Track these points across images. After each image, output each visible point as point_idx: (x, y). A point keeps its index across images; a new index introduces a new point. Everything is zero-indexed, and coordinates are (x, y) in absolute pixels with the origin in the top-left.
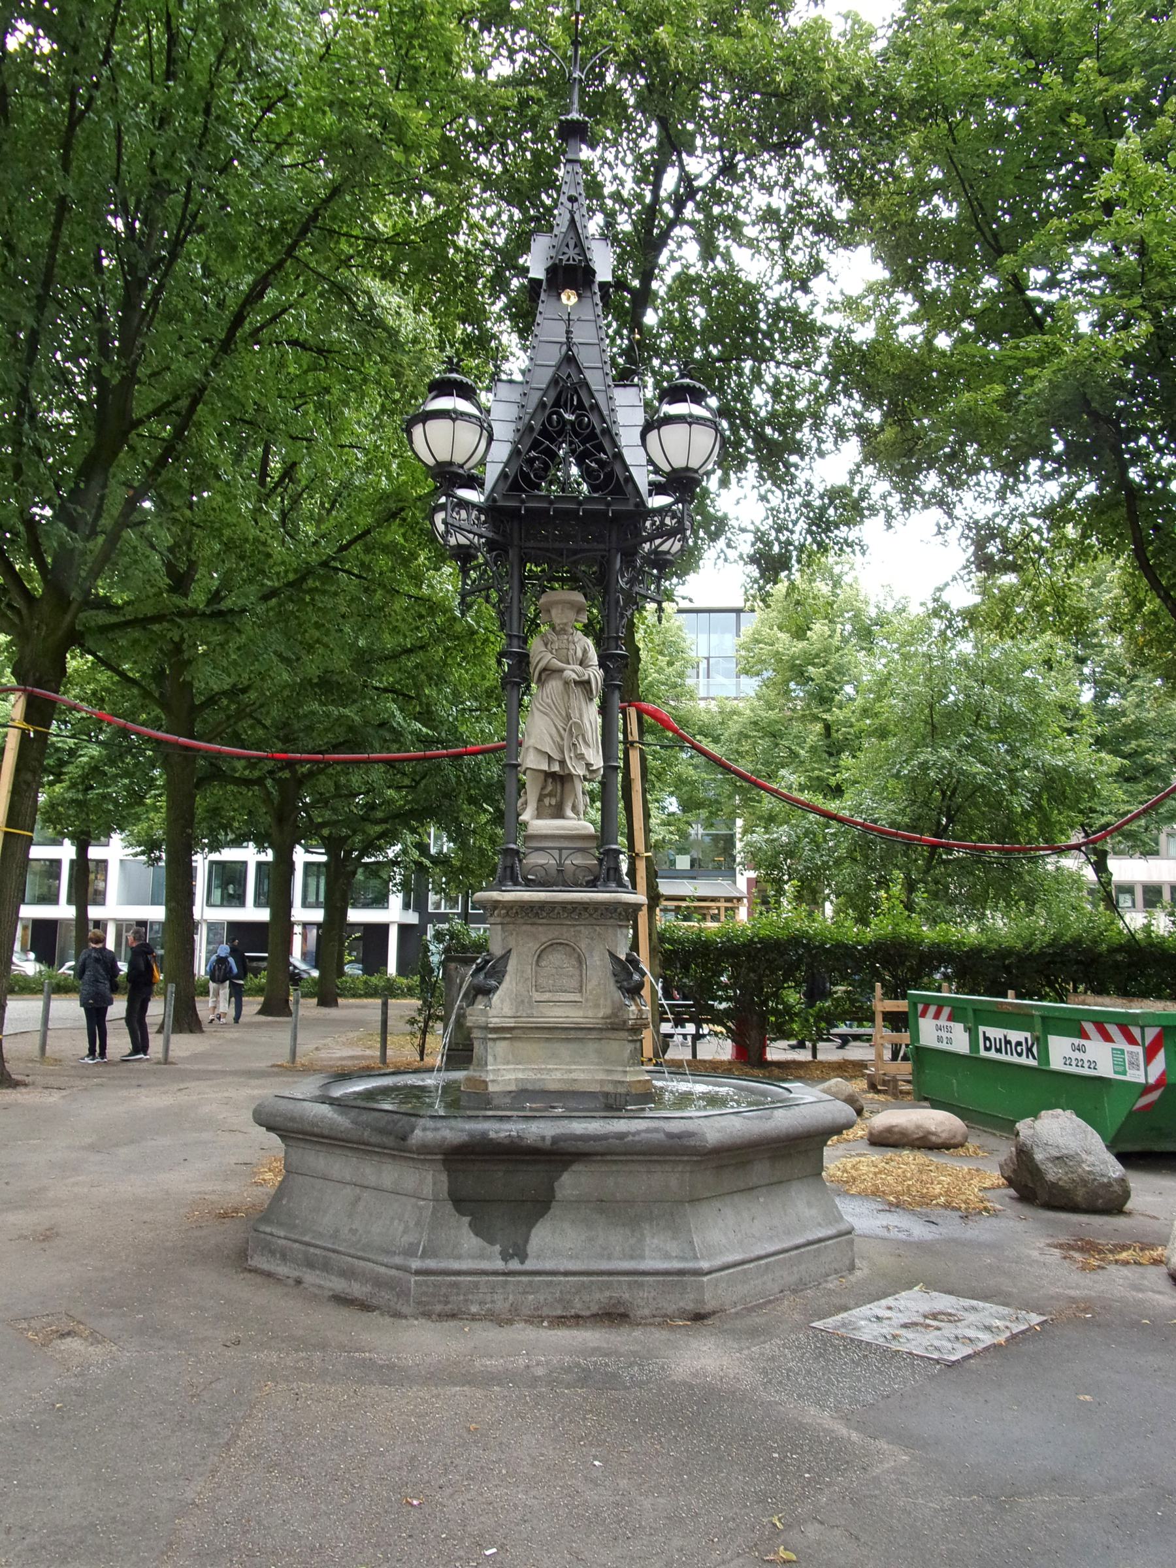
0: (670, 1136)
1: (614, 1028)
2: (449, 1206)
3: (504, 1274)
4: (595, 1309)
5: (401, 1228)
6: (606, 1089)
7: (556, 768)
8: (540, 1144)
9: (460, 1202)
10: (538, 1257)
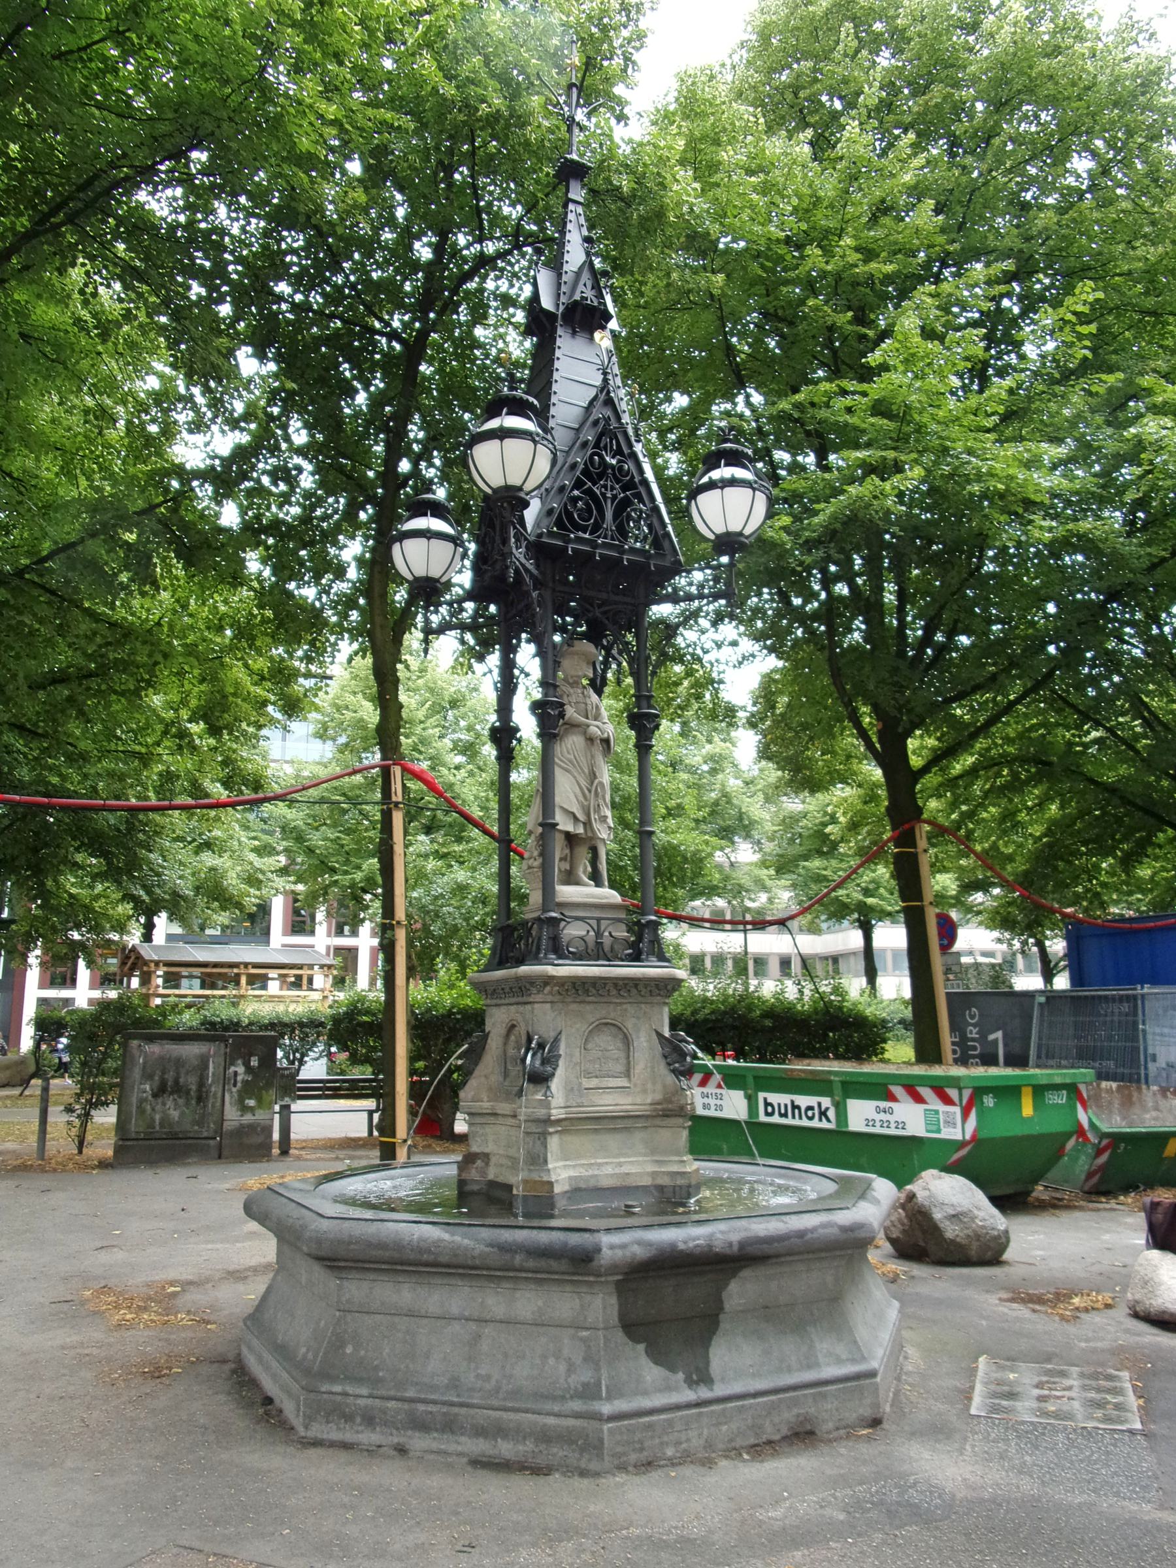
0: (845, 1229)
1: (666, 1114)
2: (620, 1335)
3: (698, 1405)
4: (785, 1431)
5: (562, 1368)
6: (660, 1181)
7: (580, 830)
8: (728, 1251)
9: (633, 1327)
10: (723, 1380)
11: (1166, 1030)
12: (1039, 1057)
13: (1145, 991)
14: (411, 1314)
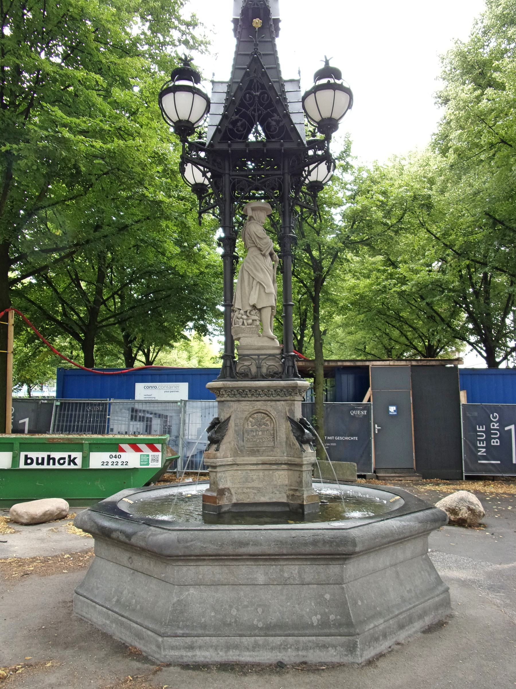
11: (120, 418)
12: (54, 431)
13: (112, 401)
14: (374, 571)
